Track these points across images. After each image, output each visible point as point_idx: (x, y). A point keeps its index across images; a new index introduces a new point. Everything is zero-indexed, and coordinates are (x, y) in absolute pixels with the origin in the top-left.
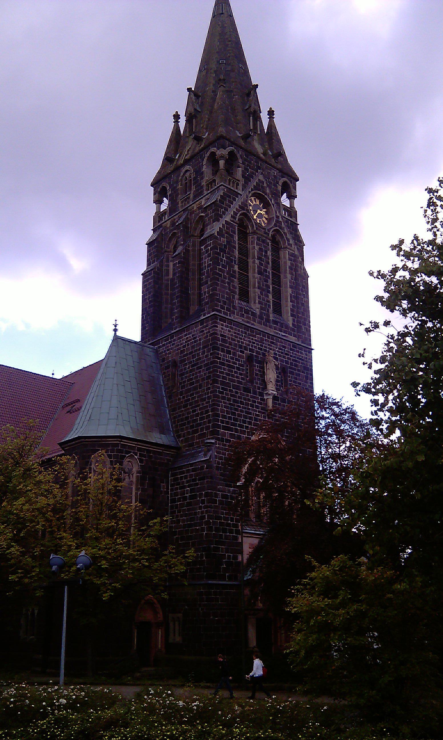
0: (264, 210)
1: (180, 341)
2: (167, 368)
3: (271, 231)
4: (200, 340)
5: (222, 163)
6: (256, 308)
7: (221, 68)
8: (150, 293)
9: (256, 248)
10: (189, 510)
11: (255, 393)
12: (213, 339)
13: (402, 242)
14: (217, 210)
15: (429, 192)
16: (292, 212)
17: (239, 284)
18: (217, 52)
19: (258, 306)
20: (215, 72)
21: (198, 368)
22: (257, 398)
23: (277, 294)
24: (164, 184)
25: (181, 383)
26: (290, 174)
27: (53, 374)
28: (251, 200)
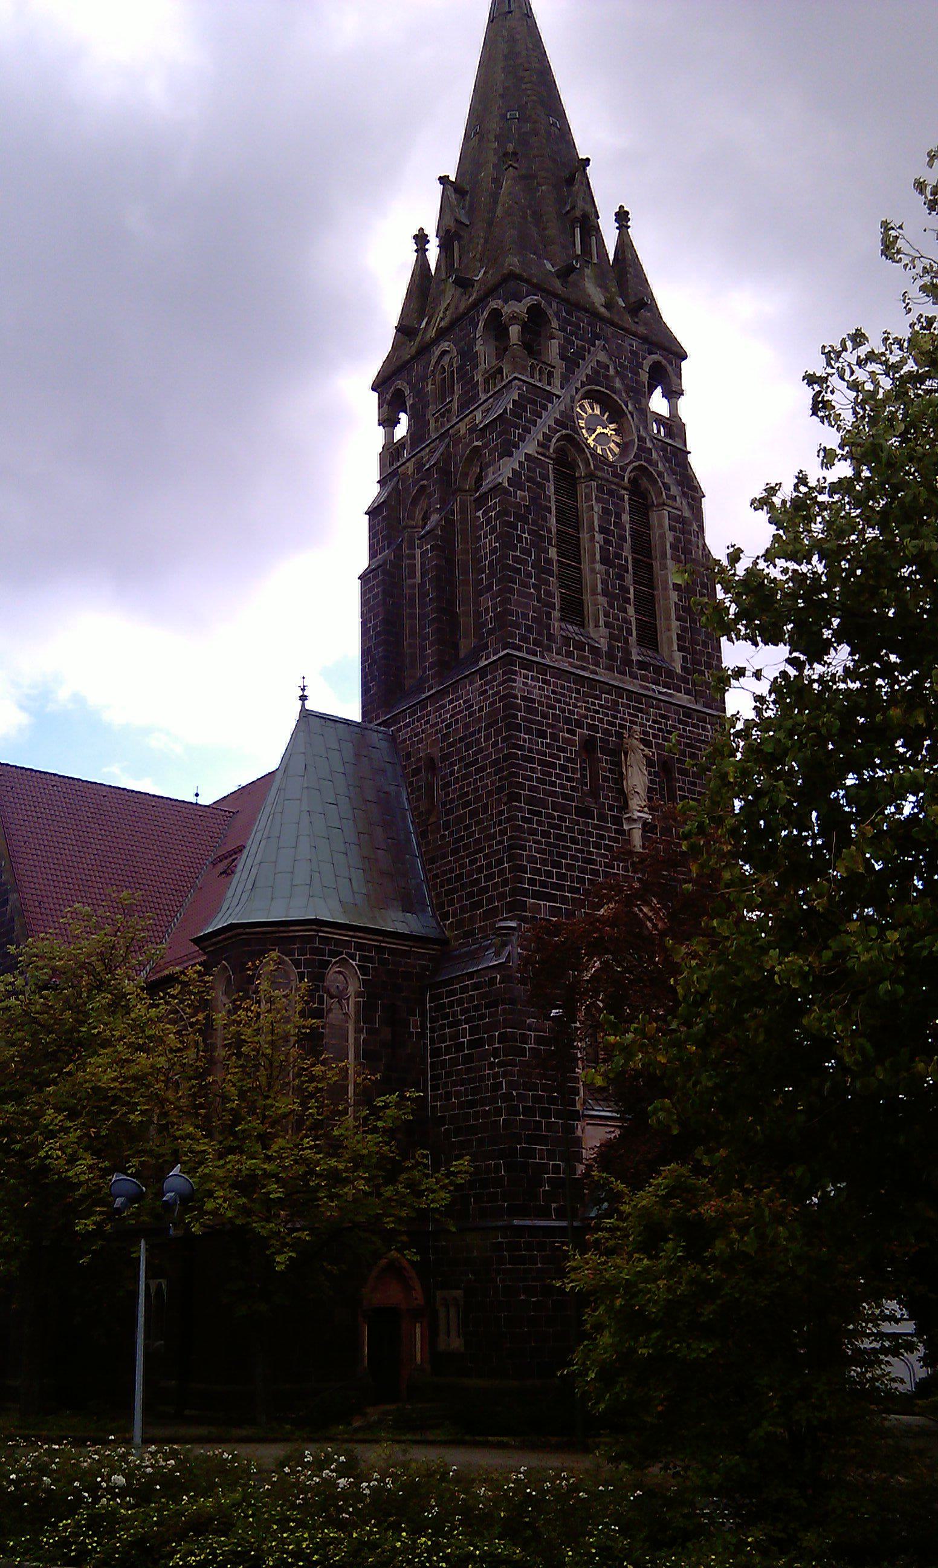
0: (612, 426)
1: (440, 715)
2: (416, 772)
3: (629, 470)
4: (481, 709)
5: (514, 331)
6: (600, 636)
7: (510, 129)
8: (376, 616)
9: (596, 509)
10: (469, 1070)
11: (602, 817)
12: (506, 707)
13: (772, 490)
14: (505, 433)
15: (810, 384)
16: (674, 427)
17: (561, 587)
18: (502, 96)
19: (603, 630)
20: (497, 138)
21: (478, 771)
22: (609, 829)
23: (647, 604)
24: (400, 384)
25: (444, 804)
26: (667, 344)
27: (197, 795)
28: (582, 407)
